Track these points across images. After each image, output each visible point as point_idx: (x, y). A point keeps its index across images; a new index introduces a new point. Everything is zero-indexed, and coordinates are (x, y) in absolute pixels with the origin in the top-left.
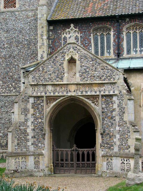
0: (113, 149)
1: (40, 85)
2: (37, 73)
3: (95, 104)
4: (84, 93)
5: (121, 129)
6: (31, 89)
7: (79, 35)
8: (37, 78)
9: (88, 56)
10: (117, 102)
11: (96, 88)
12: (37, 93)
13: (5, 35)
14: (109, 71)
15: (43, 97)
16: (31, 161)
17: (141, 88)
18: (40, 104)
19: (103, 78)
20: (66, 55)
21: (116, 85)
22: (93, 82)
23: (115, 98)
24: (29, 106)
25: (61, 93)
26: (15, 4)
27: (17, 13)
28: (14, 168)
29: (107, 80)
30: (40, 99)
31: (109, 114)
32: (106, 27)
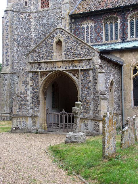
0: (89, 113)
1: (36, 63)
2: (34, 54)
3: (76, 77)
4: (68, 68)
5: (94, 97)
7: (93, 25)
8: (35, 57)
9: (71, 38)
10: (92, 74)
11: (76, 64)
13: (41, 28)
14: (87, 49)
15: (38, 72)
16: (29, 121)
17: (132, 65)
18: (36, 78)
19: (82, 55)
20: (55, 38)
21: (92, 61)
22: (74, 59)
23: (91, 72)
24: (29, 79)
25: (51, 68)
26: (48, 4)
27: (49, 11)
28: (16, 126)
29: (85, 57)
30: (36, 74)
31: (86, 85)
32: (114, 17)
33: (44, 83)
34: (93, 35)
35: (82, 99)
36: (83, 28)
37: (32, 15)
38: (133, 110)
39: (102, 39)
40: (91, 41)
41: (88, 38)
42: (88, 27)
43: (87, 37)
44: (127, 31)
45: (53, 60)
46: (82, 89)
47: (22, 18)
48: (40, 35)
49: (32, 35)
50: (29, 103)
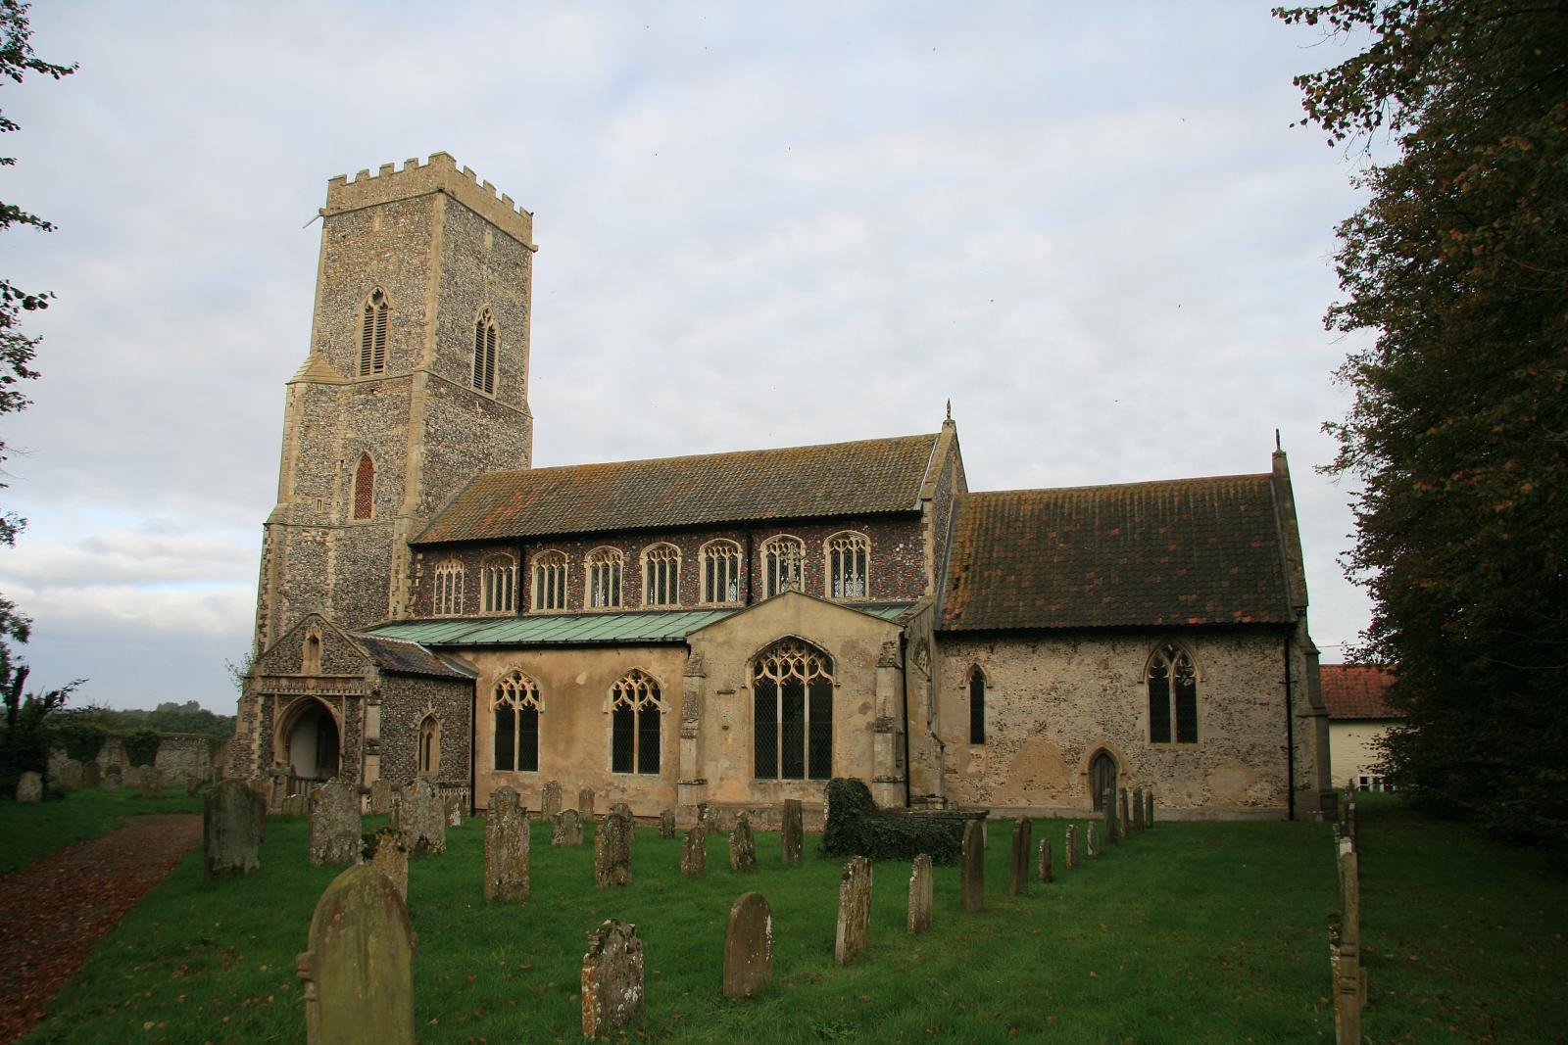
6: (262, 683)
7: (462, 571)
12: (268, 689)
13: (351, 568)
24: (258, 709)
27: (371, 528)
33: (284, 717)
35: (346, 753)
36: (440, 576)
37: (332, 533)
38: (493, 779)
42: (450, 575)
43: (448, 600)
44: (528, 592)
45: (302, 675)
46: (346, 734)
47: (306, 542)
49: (328, 582)
50: (255, 757)
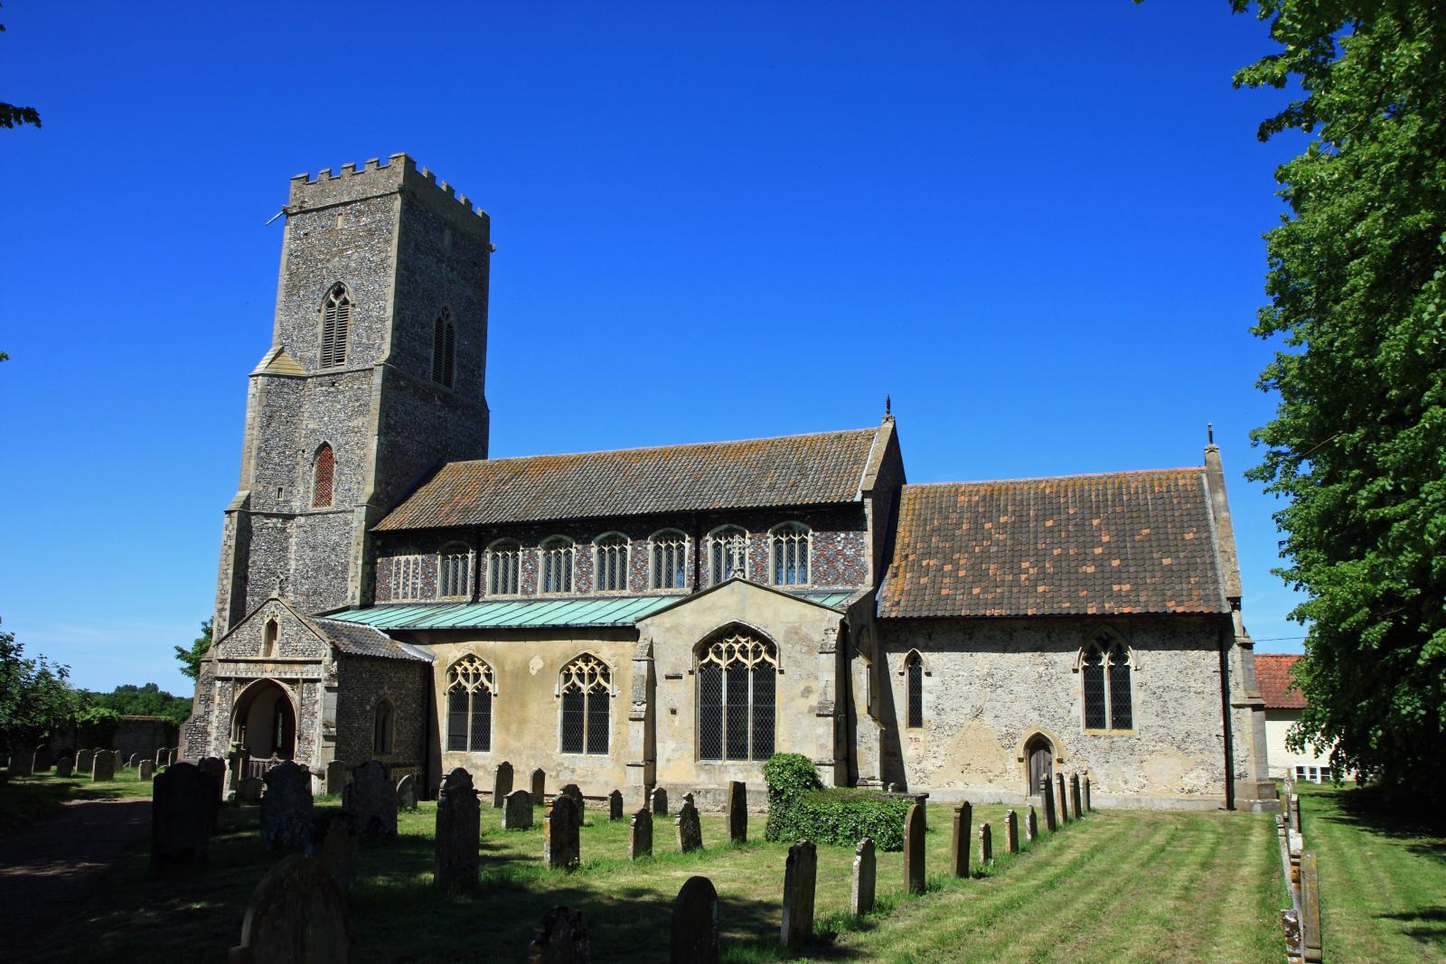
13: (311, 554)
34: (417, 581)
39: (434, 591)
40: (412, 593)
41: (408, 585)
42: (408, 562)
48: (307, 571)
